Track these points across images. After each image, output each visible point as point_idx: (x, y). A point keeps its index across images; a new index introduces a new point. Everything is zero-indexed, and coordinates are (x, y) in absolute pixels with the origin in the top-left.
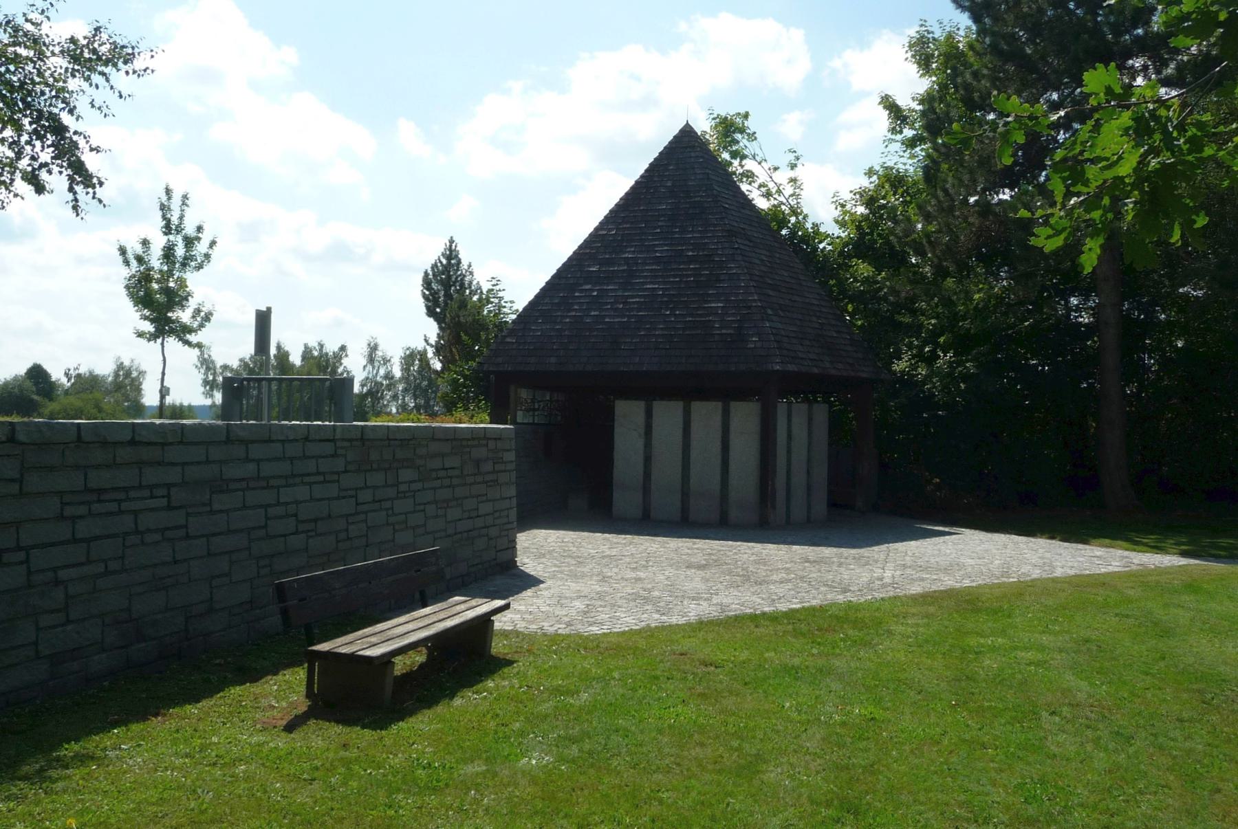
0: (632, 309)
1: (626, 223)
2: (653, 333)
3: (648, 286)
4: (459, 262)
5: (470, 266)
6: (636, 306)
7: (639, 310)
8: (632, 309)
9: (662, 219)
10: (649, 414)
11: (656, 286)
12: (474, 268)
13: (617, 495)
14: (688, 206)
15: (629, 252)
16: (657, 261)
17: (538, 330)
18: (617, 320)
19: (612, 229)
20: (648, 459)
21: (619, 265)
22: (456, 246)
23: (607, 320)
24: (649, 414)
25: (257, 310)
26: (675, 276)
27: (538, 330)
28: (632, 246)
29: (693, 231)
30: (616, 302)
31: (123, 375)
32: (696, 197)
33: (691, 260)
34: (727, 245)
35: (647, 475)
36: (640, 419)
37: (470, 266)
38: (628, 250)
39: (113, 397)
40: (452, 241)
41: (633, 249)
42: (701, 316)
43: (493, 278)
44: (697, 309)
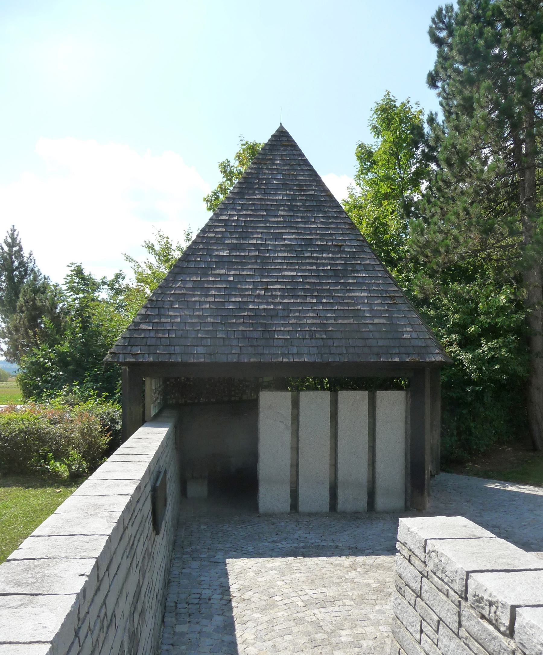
0: (276, 296)
1: (247, 210)
2: (304, 321)
3: (286, 273)
4: (21, 249)
5: (31, 254)
6: (279, 293)
7: (283, 297)
8: (276, 296)
9: (282, 208)
10: (295, 404)
11: (295, 274)
12: (35, 256)
13: (263, 490)
14: (304, 198)
15: (257, 238)
16: (289, 248)
17: (175, 317)
18: (262, 307)
19: (233, 215)
20: (296, 449)
21: (249, 251)
22: (18, 235)
23: (251, 307)
24: (295, 404)
25: (361, 146)
26: (311, 264)
27: (175, 317)
28: (258, 233)
29: (314, 222)
30: (255, 289)
31: (99, 384)
32: (309, 190)
33: (323, 249)
34: (353, 237)
35: (295, 466)
36: (287, 411)
37: (31, 254)
38: (255, 236)
39: (287, 612)
40: (13, 230)
41: (260, 236)
42: (348, 304)
43: (73, 264)
44: (343, 298)
